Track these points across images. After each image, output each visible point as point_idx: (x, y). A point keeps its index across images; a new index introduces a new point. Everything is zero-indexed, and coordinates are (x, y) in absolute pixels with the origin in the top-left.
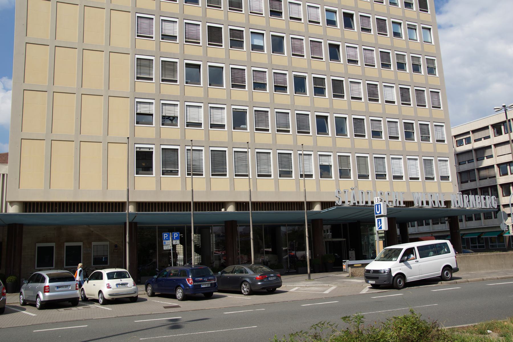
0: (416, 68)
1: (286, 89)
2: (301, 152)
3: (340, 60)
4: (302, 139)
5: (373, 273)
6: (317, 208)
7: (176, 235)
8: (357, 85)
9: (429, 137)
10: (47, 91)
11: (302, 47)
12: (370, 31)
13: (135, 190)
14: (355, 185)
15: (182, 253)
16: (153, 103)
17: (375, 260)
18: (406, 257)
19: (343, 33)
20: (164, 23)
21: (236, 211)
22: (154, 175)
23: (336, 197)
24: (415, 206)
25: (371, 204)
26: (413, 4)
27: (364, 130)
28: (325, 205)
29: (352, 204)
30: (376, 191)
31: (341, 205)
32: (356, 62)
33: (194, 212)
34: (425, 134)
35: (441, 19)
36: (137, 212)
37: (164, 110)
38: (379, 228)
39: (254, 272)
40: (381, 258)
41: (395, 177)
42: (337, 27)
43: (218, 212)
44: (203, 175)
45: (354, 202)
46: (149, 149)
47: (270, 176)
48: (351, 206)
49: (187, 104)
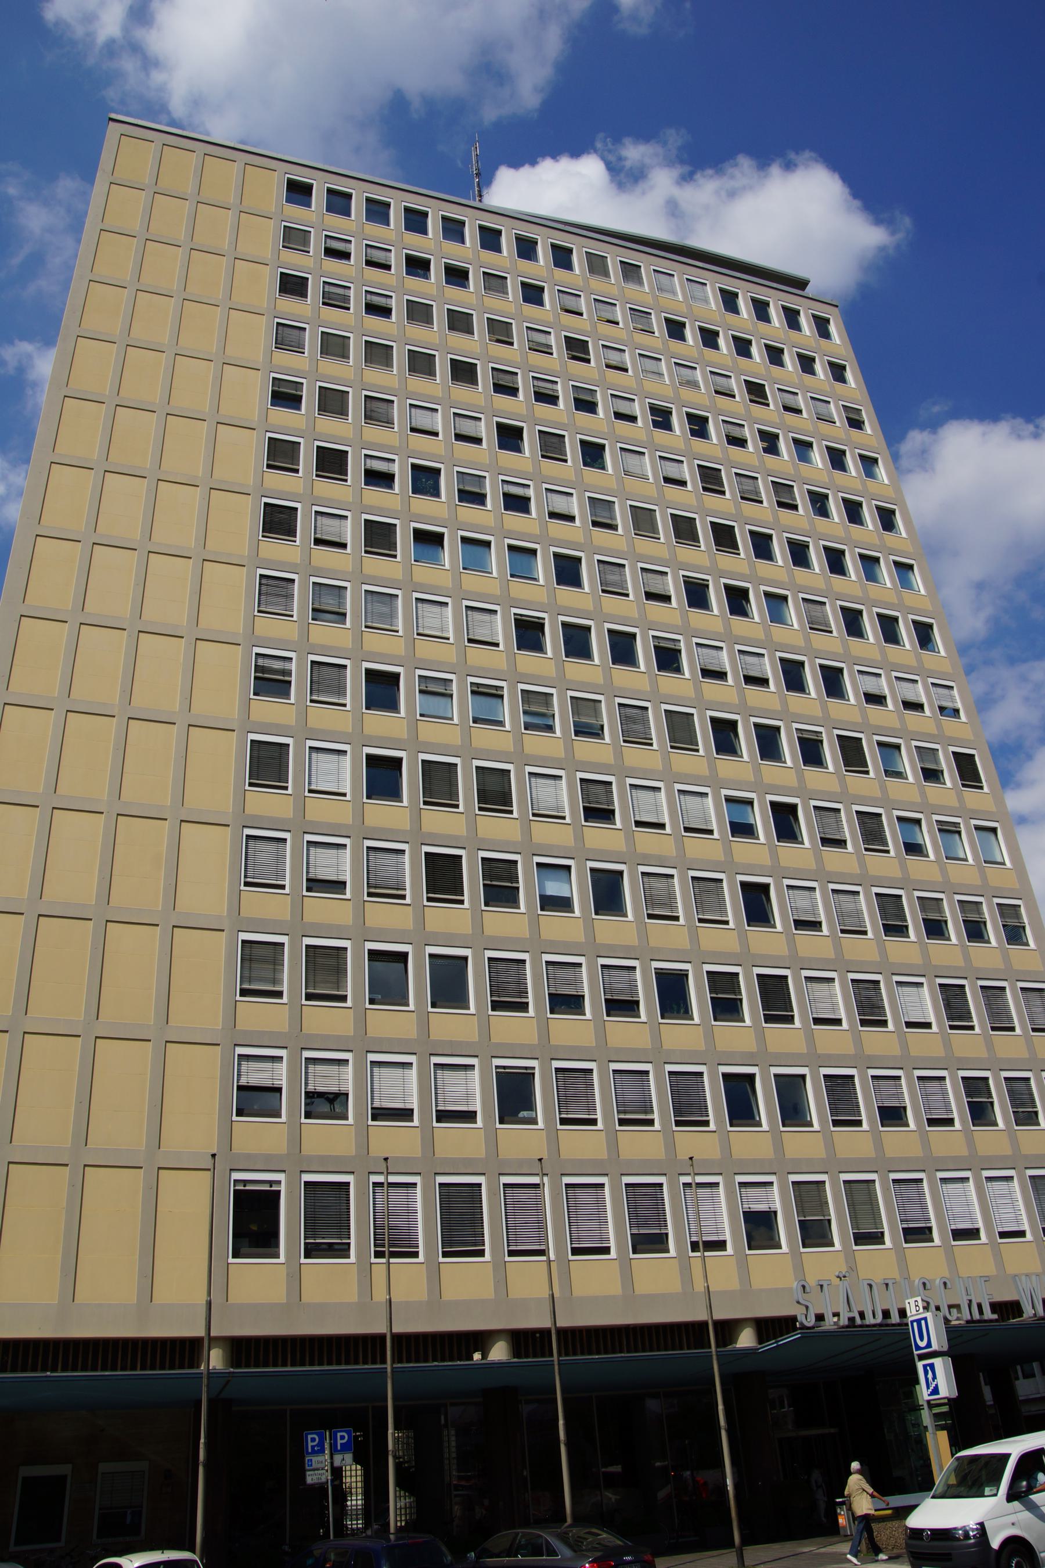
0: (975, 931)
1: (635, 1006)
2: (687, 1179)
3: (773, 923)
4: (689, 1140)
5: (932, 1539)
6: (746, 1339)
7: (342, 1437)
8: (824, 986)
9: (1036, 1113)
10: (7, 1031)
11: (672, 897)
12: (843, 844)
13: (229, 1302)
14: (847, 1262)
15: (360, 1491)
16: (282, 1057)
17: (932, 1493)
18: (1024, 1483)
19: (774, 853)
20: (312, 850)
21: (514, 1358)
22: (282, 1259)
23: (798, 1302)
24: (1025, 1316)
25: (900, 1318)
26: (942, 772)
27: (858, 1106)
28: (767, 1328)
29: (844, 1321)
30: (908, 1278)
31: (813, 1327)
32: (816, 925)
33: (395, 1366)
34: (1023, 1105)
35: (1016, 801)
36: (232, 1370)
37: (311, 1076)
38: (930, 1390)
39: (575, 1551)
40: (949, 1486)
41: (960, 1234)
42: (758, 838)
43: (462, 1363)
44: (420, 1253)
45: (851, 1315)
46: (269, 1185)
47: (606, 1250)
48: (843, 1327)
49: (372, 1057)
